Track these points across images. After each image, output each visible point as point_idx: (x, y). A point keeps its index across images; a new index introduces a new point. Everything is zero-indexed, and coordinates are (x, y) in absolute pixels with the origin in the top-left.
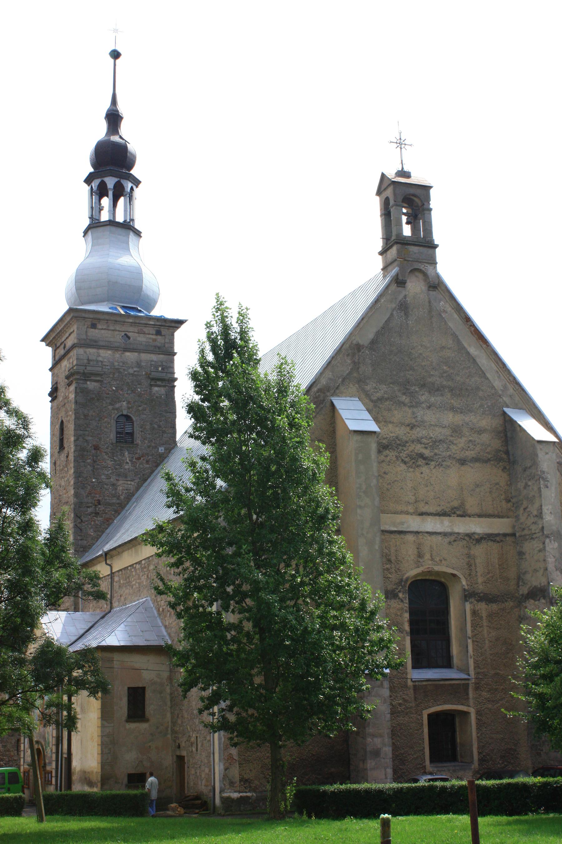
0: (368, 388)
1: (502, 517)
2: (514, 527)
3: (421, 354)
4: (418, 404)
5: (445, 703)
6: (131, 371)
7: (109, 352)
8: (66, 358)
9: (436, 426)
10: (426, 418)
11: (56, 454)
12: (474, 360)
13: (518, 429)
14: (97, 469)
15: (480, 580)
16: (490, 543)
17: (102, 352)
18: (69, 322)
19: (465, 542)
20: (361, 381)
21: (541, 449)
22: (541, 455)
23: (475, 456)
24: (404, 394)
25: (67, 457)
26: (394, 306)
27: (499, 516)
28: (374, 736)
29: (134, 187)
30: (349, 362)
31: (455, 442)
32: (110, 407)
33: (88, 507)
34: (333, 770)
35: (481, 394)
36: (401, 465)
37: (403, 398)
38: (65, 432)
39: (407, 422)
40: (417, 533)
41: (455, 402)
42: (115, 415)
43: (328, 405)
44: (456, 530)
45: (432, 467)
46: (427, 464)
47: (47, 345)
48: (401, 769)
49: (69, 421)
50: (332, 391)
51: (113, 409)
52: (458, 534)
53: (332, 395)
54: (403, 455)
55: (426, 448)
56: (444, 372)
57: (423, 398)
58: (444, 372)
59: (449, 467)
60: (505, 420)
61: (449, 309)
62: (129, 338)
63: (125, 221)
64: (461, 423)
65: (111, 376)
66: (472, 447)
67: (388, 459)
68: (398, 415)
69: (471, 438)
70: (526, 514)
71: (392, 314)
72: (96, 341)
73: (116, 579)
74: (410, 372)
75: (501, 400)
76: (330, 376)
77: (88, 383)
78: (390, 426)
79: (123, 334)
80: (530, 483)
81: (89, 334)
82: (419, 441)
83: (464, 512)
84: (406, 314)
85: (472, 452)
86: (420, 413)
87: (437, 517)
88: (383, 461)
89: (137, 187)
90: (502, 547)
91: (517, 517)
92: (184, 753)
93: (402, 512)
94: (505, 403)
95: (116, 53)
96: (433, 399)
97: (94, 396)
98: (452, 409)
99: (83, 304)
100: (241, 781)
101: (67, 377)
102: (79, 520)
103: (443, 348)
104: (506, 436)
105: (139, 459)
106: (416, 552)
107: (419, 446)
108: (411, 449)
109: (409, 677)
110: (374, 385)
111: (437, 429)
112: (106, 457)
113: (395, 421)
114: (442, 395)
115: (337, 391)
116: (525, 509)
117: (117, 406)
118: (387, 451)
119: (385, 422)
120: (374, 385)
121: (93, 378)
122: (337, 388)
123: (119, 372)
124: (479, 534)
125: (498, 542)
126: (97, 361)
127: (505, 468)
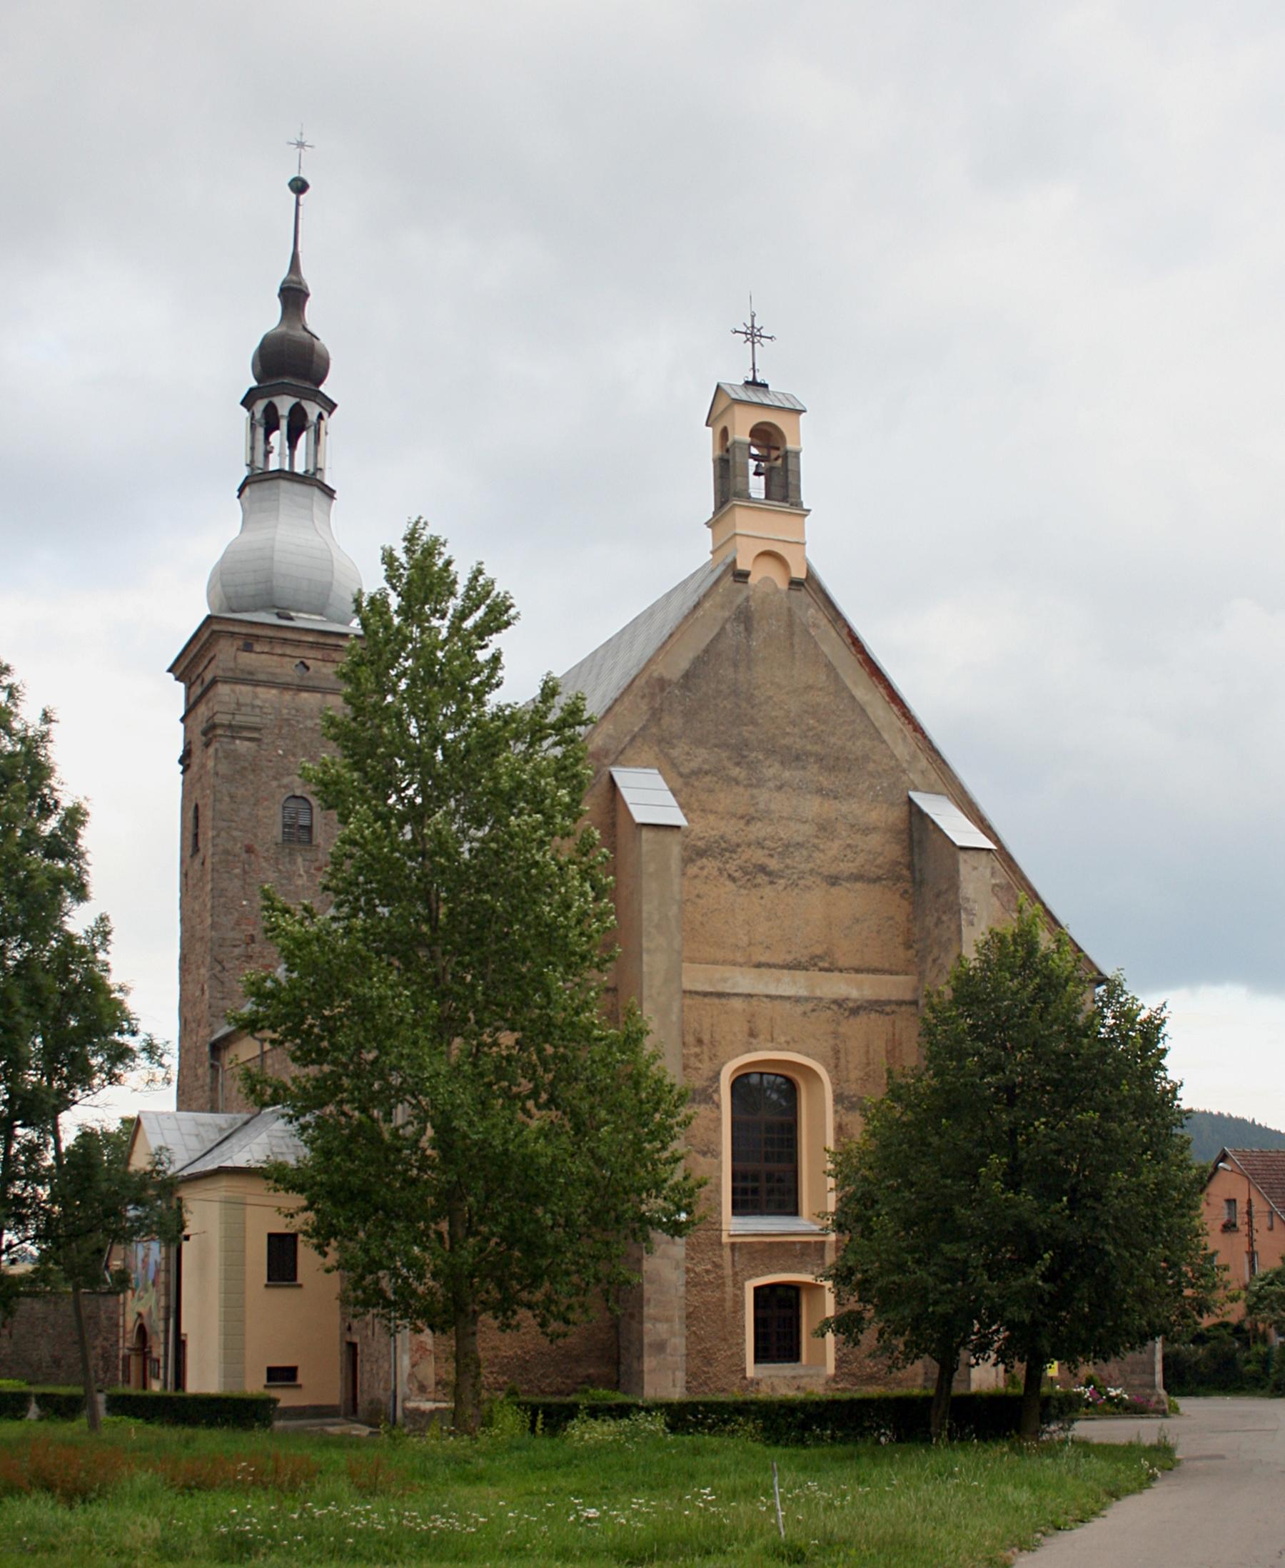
0: (675, 753)
1: (897, 973)
2: (916, 990)
3: (770, 698)
4: (760, 783)
5: (784, 1270)
6: (310, 723)
7: (274, 691)
8: (204, 701)
9: (790, 819)
10: (773, 807)
11: (188, 860)
12: (863, 710)
13: (931, 827)
14: (250, 884)
15: (855, 1074)
16: (873, 1015)
17: (261, 691)
18: (207, 640)
19: (829, 1013)
20: (664, 741)
21: (965, 861)
22: (964, 869)
23: (855, 871)
24: (738, 764)
25: (203, 864)
26: (727, 614)
27: (891, 973)
28: (656, 1319)
29: (325, 414)
30: (644, 708)
31: (821, 847)
32: (274, 784)
33: (235, 946)
34: (591, 1371)
35: (871, 767)
36: (728, 883)
37: (736, 771)
38: (201, 823)
39: (740, 811)
40: (750, 996)
41: (825, 781)
42: (282, 795)
43: (605, 779)
44: (818, 993)
45: (780, 888)
46: (771, 883)
47: (177, 679)
48: (705, 1372)
49: (205, 805)
50: (612, 757)
51: (279, 786)
52: (820, 999)
53: (613, 764)
54: (731, 867)
55: (771, 856)
56: (810, 729)
57: (770, 773)
58: (810, 729)
59: (809, 888)
60: (910, 812)
61: (824, 622)
62: (307, 668)
63: (306, 472)
64: (833, 815)
65: (276, 731)
66: (850, 855)
67: (705, 872)
68: (726, 799)
69: (849, 841)
70: (935, 971)
71: (723, 629)
72: (251, 673)
73: (269, 1062)
74: (751, 728)
75: (905, 778)
76: (611, 732)
77: (238, 742)
78: (711, 817)
79: (297, 661)
80: (944, 918)
81: (240, 661)
82: (760, 845)
83: (831, 963)
84: (748, 630)
85: (850, 865)
86: (763, 796)
87: (785, 971)
88: (696, 877)
89: (330, 413)
90: (894, 1023)
91: (921, 975)
92: (356, 1339)
93: (724, 962)
94: (913, 782)
95: (300, 183)
96: (787, 774)
97: (246, 764)
98: (819, 791)
99: (234, 611)
100: (437, 1383)
101: (205, 733)
102: (219, 968)
103: (809, 687)
104: (911, 837)
105: (319, 869)
106: (746, 1028)
107: (760, 852)
108: (744, 857)
109: (724, 1227)
110: (687, 748)
111: (792, 824)
112: (264, 864)
113: (720, 809)
114: (804, 768)
115: (621, 758)
116: (934, 961)
117: (286, 781)
118: (704, 860)
119: (703, 810)
120: (687, 748)
121: (246, 734)
122: (622, 752)
123: (290, 725)
124: (855, 1001)
125: (887, 1014)
126: (253, 707)
127: (906, 892)
